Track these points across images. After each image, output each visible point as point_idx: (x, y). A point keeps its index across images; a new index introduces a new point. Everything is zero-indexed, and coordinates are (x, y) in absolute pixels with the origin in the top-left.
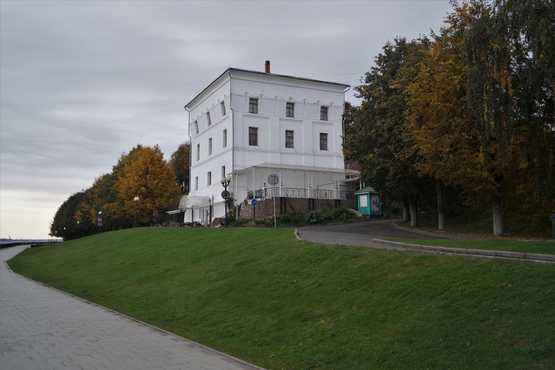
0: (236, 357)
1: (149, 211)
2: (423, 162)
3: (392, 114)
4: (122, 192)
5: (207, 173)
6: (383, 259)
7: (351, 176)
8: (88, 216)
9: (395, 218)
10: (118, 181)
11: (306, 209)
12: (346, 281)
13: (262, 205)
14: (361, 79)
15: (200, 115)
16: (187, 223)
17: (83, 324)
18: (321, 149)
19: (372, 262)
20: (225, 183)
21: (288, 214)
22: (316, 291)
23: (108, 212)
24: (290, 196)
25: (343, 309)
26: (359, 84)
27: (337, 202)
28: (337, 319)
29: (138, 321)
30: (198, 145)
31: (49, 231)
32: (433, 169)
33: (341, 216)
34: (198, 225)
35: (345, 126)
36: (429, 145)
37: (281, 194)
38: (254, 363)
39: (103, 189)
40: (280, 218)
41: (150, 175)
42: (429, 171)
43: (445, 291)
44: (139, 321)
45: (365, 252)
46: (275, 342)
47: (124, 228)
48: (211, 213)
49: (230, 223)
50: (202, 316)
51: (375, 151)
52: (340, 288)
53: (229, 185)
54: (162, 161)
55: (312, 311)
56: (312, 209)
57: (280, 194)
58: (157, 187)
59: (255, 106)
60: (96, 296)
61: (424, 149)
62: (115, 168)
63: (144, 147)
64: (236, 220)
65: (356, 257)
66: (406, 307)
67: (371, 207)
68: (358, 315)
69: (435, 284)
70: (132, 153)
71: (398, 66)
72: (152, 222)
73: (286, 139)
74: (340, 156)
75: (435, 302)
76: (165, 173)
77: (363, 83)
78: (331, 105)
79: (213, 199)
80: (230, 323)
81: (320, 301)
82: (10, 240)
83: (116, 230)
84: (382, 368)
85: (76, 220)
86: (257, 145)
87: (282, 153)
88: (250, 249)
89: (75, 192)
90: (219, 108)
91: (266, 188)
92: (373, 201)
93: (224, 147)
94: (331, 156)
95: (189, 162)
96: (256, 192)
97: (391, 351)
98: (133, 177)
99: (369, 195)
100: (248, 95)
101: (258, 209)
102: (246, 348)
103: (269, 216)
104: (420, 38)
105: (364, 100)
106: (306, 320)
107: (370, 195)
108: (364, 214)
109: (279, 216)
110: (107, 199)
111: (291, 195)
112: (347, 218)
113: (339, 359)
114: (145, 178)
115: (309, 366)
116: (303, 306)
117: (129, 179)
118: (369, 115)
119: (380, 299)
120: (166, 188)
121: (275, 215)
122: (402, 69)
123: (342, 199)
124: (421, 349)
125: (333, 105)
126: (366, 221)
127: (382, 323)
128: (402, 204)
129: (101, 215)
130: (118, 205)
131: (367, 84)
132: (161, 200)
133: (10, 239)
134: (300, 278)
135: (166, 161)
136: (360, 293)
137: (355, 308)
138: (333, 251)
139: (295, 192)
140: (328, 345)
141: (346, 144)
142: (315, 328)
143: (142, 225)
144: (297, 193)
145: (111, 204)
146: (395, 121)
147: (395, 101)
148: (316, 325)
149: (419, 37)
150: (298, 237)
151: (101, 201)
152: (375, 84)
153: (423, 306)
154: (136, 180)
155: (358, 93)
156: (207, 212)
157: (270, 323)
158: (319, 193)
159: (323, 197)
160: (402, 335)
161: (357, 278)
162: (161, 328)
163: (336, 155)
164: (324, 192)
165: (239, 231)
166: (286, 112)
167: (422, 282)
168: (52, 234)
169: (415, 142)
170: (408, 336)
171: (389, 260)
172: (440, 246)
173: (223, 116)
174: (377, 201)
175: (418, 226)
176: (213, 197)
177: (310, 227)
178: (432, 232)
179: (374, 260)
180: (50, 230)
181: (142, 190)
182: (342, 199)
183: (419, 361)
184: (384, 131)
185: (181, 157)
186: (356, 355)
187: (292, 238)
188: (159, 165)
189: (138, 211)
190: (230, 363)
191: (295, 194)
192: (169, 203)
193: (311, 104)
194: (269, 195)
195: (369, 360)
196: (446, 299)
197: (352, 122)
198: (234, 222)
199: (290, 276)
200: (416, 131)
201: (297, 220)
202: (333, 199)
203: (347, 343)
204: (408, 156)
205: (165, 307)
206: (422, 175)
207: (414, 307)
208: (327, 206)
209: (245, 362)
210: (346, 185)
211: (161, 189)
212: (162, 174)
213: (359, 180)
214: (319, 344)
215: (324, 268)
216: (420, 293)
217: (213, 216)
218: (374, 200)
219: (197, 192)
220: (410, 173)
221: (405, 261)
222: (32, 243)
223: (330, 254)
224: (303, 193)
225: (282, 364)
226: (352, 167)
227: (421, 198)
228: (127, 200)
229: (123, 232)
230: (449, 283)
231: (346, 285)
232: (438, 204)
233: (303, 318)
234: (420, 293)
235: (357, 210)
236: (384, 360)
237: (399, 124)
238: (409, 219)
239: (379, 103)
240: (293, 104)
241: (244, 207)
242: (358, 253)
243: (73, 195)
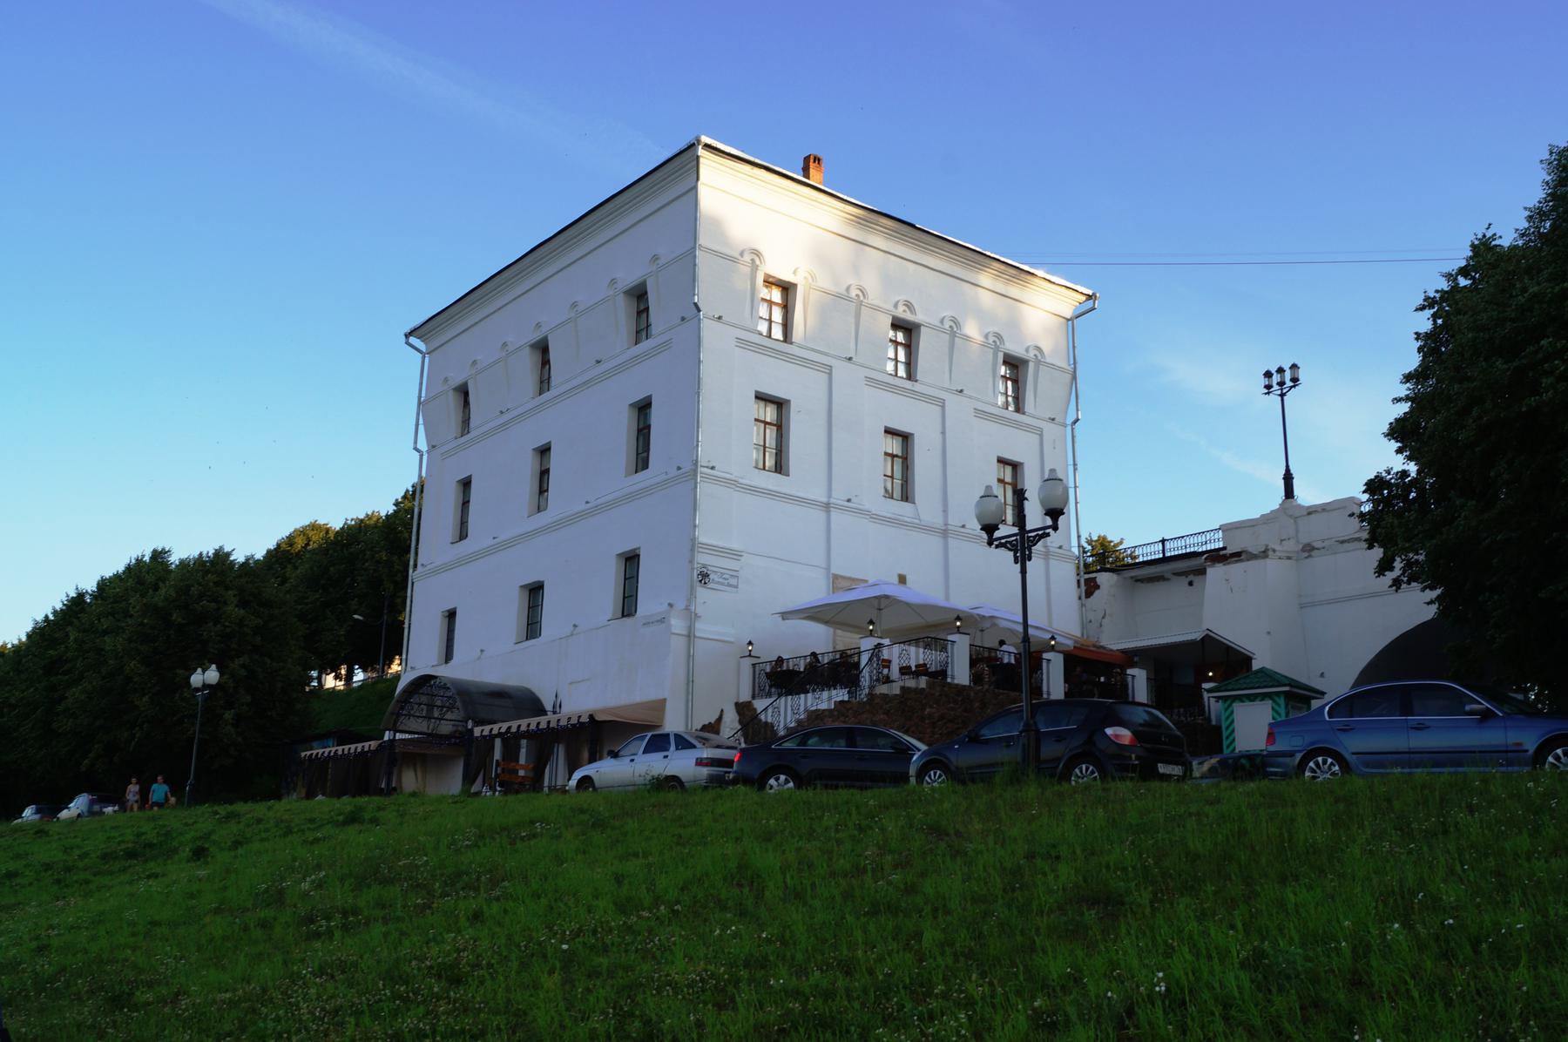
53: (1055, 528)
107: (1286, 698)
243: (1424, 323)
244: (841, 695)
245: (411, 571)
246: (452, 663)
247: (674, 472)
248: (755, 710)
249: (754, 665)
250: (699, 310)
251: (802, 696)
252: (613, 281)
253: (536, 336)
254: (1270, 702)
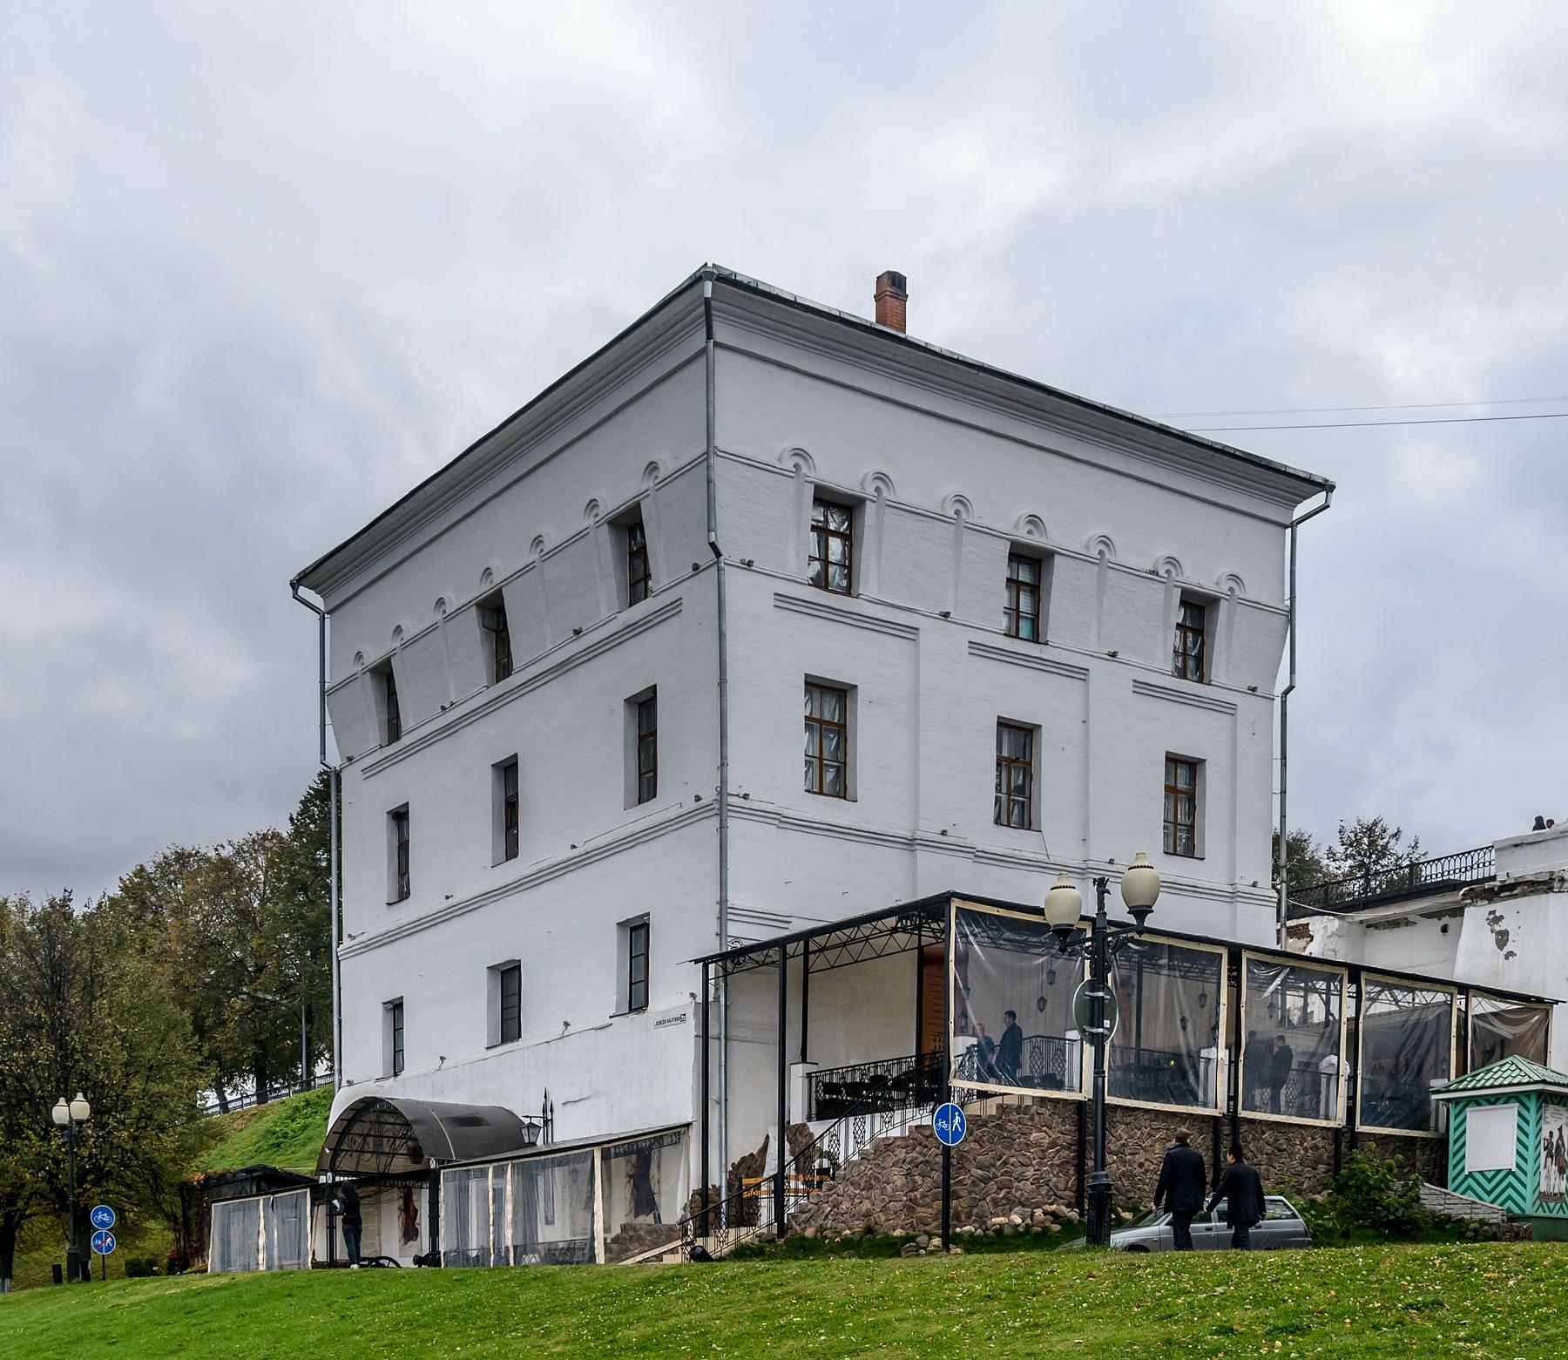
244: (923, 1117)
245: (334, 944)
246: (403, 1075)
247: (692, 805)
248: (812, 1135)
249: (809, 1076)
250: (718, 554)
251: (868, 1117)
252: (593, 504)
253: (483, 589)
254: (1518, 1104)
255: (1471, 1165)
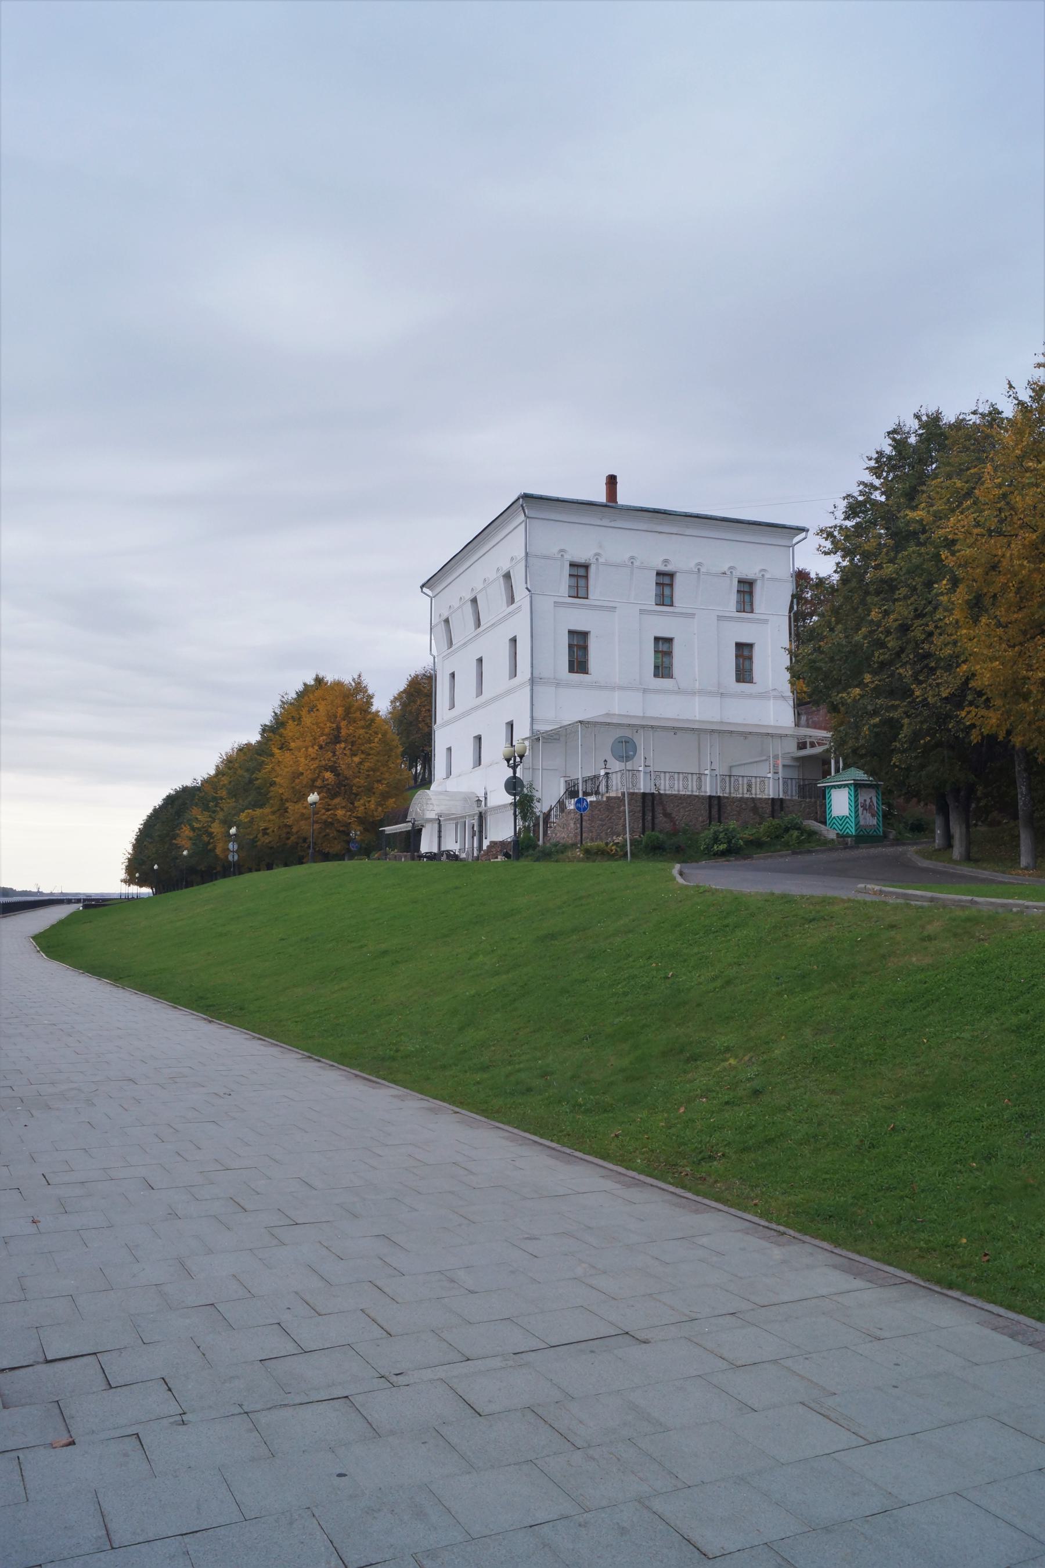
0: (535, 1134)
1: (342, 826)
2: (983, 706)
3: (908, 591)
4: (282, 787)
5: (472, 740)
6: (878, 923)
7: (810, 742)
8: (205, 838)
9: (916, 844)
10: (271, 758)
11: (703, 822)
12: (788, 974)
13: (599, 810)
14: (832, 509)
15: (456, 604)
16: (427, 853)
17: (200, 1062)
18: (738, 680)
19: (851, 931)
20: (513, 760)
21: (661, 832)
22: (718, 995)
23: (250, 829)
24: (665, 790)
25: (782, 1035)
26: (829, 522)
27: (777, 805)
28: (765, 1057)
29: (316, 1058)
30: (450, 674)
31: (122, 874)
32: (1006, 721)
33: (786, 837)
34: (453, 857)
35: (795, 626)
36: (998, 662)
37: (643, 786)
38: (575, 1147)
39: (240, 779)
40: (642, 841)
41: (343, 745)
42: (998, 726)
43: (1022, 993)
44: (321, 1059)
45: (836, 908)
46: (624, 1104)
47: (286, 865)
48: (480, 831)
49: (526, 854)
50: (460, 1049)
51: (866, 681)
52: (775, 989)
54: (370, 713)
55: (709, 1038)
56: (717, 820)
57: (642, 787)
58: (360, 772)
59: (582, 582)
60: (226, 1008)
61: (985, 676)
62: (265, 730)
63: (329, 682)
64: (539, 846)
65: (814, 919)
66: (927, 1030)
67: (857, 817)
68: (815, 1047)
69: (998, 978)
70: (300, 695)
71: (922, 479)
72: (349, 850)
73: (656, 658)
74: (783, 697)
75: (997, 1019)
76: (376, 740)
77: (839, 519)
78: (763, 575)
79: (486, 798)
80: (522, 1066)
81: (727, 1017)
82: (39, 893)
83: (268, 870)
84: (867, 1161)
85: (179, 847)
86: (587, 673)
87: (645, 691)
88: (569, 905)
89: (178, 785)
90: (499, 588)
91: (608, 771)
92: (863, 802)
93: (510, 678)
94: (763, 696)
95: (431, 716)
96: (585, 781)
97: (888, 1126)
98: (307, 748)
99: (852, 788)
100: (565, 557)
101: (589, 820)
102: (557, 1117)
103: (614, 838)
104: (977, 410)
105: (841, 561)
106: (694, 1058)
108: (841, 833)
109: (640, 836)
110: (250, 799)
111: (667, 788)
112: (800, 842)
113: (769, 1141)
114: (332, 752)
115: (700, 1157)
116: (688, 1027)
117: (296, 753)
118: (852, 596)
119: (866, 1012)
120: (378, 774)
121: (628, 835)
122: (933, 483)
123: (789, 798)
124: (959, 1122)
125: (767, 576)
126: (845, 848)
127: (870, 1064)
128: (933, 807)
129: (235, 835)
130: (273, 813)
131: (848, 524)
132: (370, 801)
133: (38, 892)
134: (683, 967)
135: (379, 711)
136: (820, 999)
137: (808, 1032)
138: (759, 908)
139: (676, 782)
140: (745, 1112)
141: (796, 668)
142: (714, 1077)
143: (326, 857)
144: (681, 782)
145: (258, 812)
146: (916, 610)
147: (916, 560)
148: (718, 1069)
149: (976, 408)
150: (680, 880)
151: (234, 804)
152: (866, 522)
153: (969, 1027)
154: (312, 756)
155: (828, 545)
156: (473, 828)
157: (612, 1065)
158: (732, 784)
159: (743, 794)
160: (918, 1091)
161: (815, 967)
162: (369, 1075)
163: (775, 693)
164: (745, 782)
165: (543, 870)
166: (656, 595)
167: (969, 974)
168: (130, 881)
169: (962, 658)
170: (930, 1093)
171: (892, 927)
172: (1017, 899)
173: (508, 606)
174: (871, 801)
175: (971, 860)
176: (486, 794)
177: (711, 863)
178: (1004, 872)
179: (855, 927)
180: (124, 871)
181: (326, 777)
182: (787, 798)
183: (954, 1148)
184: (888, 633)
185: (412, 704)
186: (807, 1134)
187: (666, 881)
188: (362, 723)
189: (316, 826)
190: (520, 1145)
191: (676, 786)
192: (386, 808)
193: (716, 575)
194: (614, 788)
195: (838, 1146)
196: (1022, 1013)
197: (814, 617)
198: (534, 850)
199: (661, 963)
200: (965, 631)
201: (680, 846)
202: (767, 797)
203: (789, 1109)
204: (947, 691)
205: (377, 1031)
206: (980, 737)
207: (946, 1029)
208: (752, 815)
209: (554, 1145)
210: (798, 764)
211: (368, 775)
212: (370, 741)
213: (828, 751)
214: (723, 1110)
215: (738, 945)
216: (961, 999)
217: (486, 838)
218: (865, 801)
219: (448, 781)
220: (951, 731)
221: (929, 927)
222: (85, 900)
223: (753, 915)
224: (695, 783)
225: (638, 1152)
226: (813, 722)
227: (979, 793)
228: (292, 801)
229: (282, 874)
230: (1032, 976)
231: (788, 982)
232: (1019, 808)
233: (688, 1055)
234: (962, 998)
235: (824, 823)
236: (872, 1146)
237: (924, 616)
238: (949, 845)
239: (878, 567)
240: (671, 575)
241: (556, 816)
242: (819, 912)
243: (172, 792)
255: (835, 814)
